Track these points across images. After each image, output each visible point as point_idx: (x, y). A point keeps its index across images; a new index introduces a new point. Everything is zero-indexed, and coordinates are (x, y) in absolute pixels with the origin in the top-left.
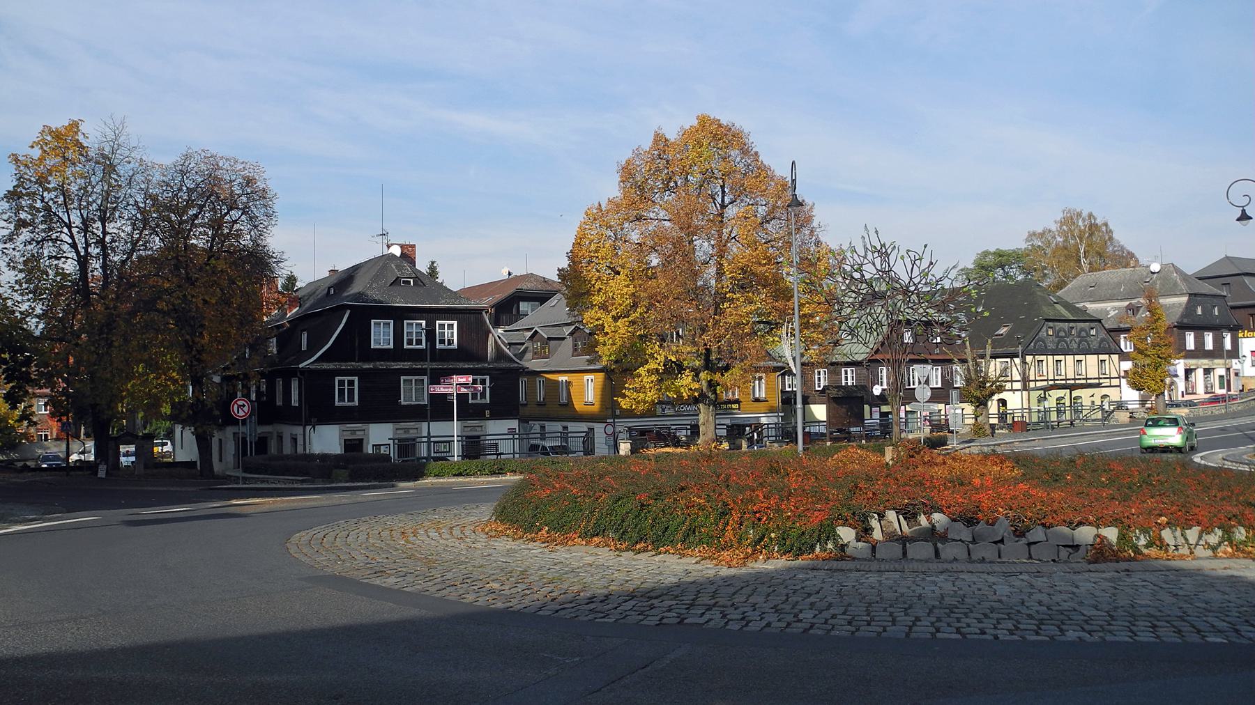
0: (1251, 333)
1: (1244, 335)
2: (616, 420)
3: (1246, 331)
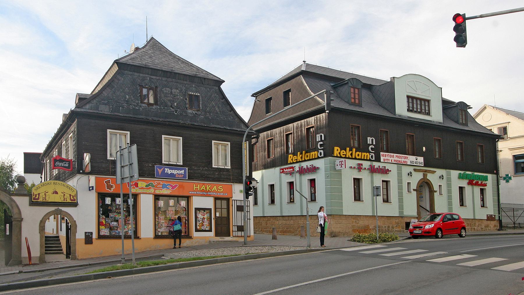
0: (360, 153)
1: (351, 154)
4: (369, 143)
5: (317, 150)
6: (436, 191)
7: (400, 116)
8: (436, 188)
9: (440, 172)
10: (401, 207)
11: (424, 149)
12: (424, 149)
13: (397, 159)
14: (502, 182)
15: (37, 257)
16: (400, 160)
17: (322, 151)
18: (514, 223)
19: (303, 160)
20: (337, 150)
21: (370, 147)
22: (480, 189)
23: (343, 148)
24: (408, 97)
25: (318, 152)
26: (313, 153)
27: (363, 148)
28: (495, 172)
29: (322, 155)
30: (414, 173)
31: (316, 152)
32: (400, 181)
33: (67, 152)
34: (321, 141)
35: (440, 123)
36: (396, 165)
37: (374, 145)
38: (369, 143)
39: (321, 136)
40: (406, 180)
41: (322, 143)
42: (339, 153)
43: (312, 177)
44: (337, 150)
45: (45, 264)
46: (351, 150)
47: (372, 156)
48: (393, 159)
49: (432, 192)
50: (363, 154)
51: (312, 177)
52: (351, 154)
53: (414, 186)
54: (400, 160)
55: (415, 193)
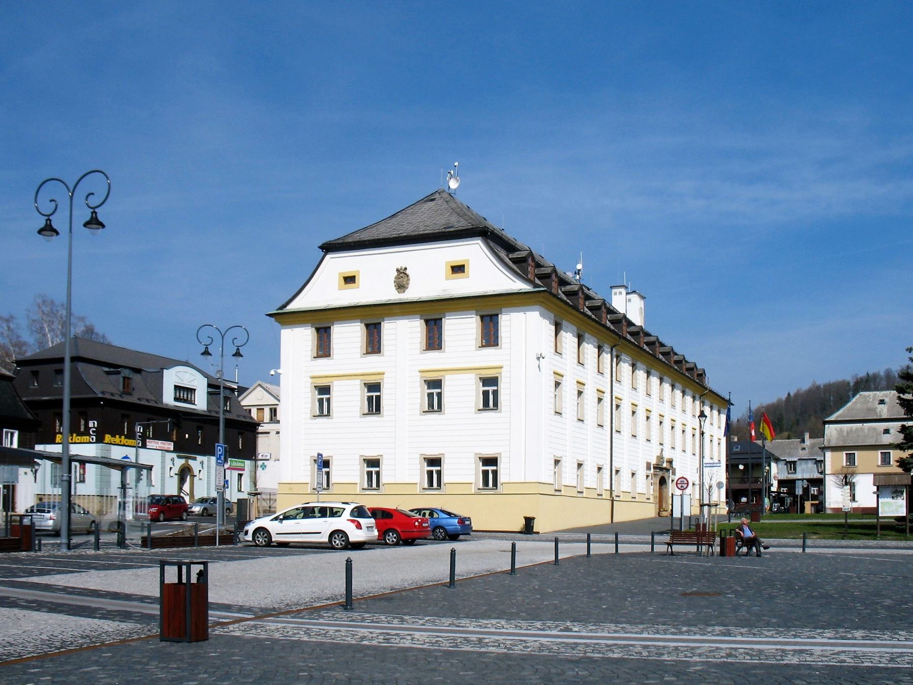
0: (79, 437)
1: (121, 441)
2: (800, 550)
3: (74, 435)
4: (90, 426)
5: (90, 435)
6: (196, 476)
7: (167, 405)
8: (196, 472)
9: (200, 458)
10: (163, 486)
11: (187, 436)
12: (187, 436)
13: (161, 445)
14: (259, 469)
15: (116, 521)
16: (164, 446)
17: (94, 437)
18: (270, 507)
19: (74, 442)
20: (108, 438)
21: (91, 430)
22: (239, 474)
23: (113, 436)
24: (176, 387)
25: (90, 437)
26: (85, 437)
27: (131, 435)
28: (254, 458)
29: (94, 441)
30: (176, 460)
31: (88, 437)
32: (163, 468)
33: (8, 445)
34: (94, 427)
35: (204, 411)
36: (160, 452)
37: (141, 433)
38: (90, 426)
39: (94, 423)
40: (169, 464)
41: (94, 429)
42: (110, 440)
43: (240, 472)
44: (108, 438)
45: (735, 558)
46: (120, 437)
47: (93, 439)
48: (158, 445)
49: (193, 476)
50: (83, 437)
51: (240, 472)
52: (121, 441)
53: (176, 470)
54: (164, 446)
55: (176, 477)
